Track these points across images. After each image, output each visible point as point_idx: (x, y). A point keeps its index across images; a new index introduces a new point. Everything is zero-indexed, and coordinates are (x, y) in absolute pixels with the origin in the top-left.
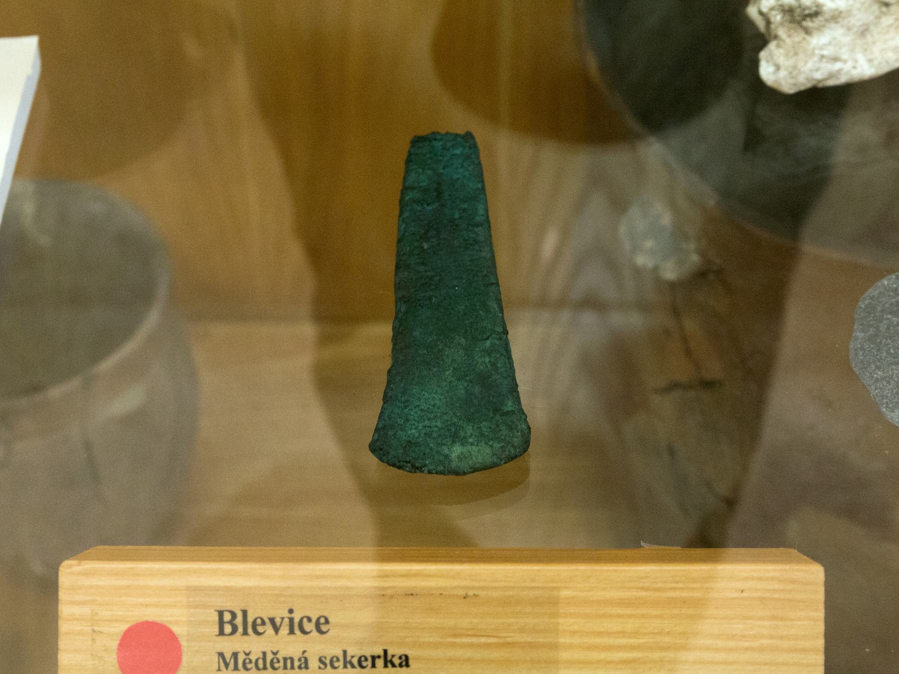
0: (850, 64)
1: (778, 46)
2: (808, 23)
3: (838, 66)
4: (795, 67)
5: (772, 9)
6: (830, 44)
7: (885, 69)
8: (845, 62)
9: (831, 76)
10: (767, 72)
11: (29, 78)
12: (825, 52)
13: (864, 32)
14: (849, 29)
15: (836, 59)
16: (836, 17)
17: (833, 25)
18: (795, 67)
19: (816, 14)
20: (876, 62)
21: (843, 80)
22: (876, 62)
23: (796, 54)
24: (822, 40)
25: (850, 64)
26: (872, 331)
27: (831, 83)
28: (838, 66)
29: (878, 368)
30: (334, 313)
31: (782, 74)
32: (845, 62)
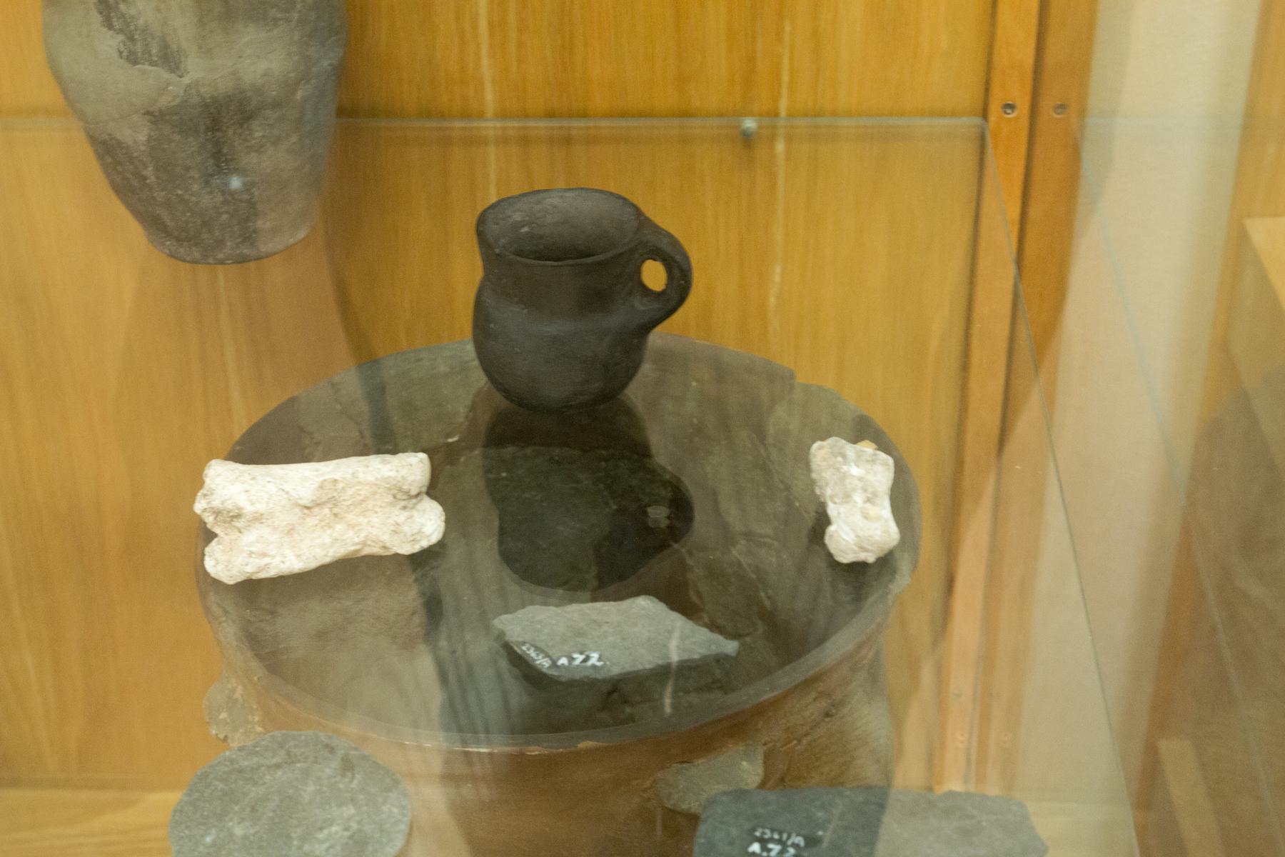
0: (278, 559)
1: (219, 543)
2: (236, 523)
3: (266, 560)
4: (229, 561)
5: (205, 510)
6: (257, 541)
7: (313, 564)
8: (273, 557)
9: (260, 570)
10: (209, 565)
11: (383, 462)
12: (254, 549)
13: (290, 531)
14: (275, 529)
15: (265, 555)
16: (258, 518)
17: (257, 525)
18: (229, 561)
19: (238, 516)
20: (304, 558)
21: (272, 573)
22: (304, 558)
23: (231, 550)
24: (251, 538)
25: (278, 559)
26: (196, 795)
27: (262, 575)
28: (266, 560)
29: (187, 827)
30: (458, 718)
31: (220, 567)
32: (273, 557)
